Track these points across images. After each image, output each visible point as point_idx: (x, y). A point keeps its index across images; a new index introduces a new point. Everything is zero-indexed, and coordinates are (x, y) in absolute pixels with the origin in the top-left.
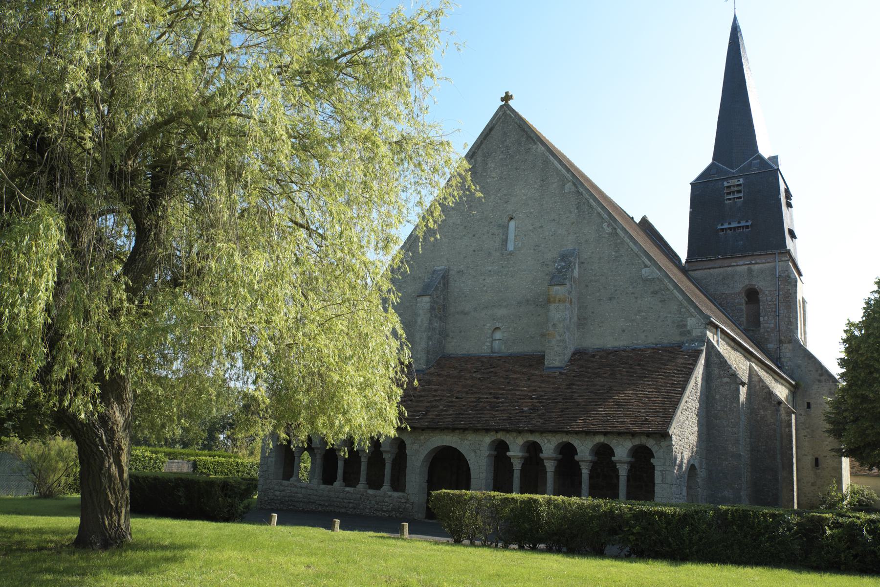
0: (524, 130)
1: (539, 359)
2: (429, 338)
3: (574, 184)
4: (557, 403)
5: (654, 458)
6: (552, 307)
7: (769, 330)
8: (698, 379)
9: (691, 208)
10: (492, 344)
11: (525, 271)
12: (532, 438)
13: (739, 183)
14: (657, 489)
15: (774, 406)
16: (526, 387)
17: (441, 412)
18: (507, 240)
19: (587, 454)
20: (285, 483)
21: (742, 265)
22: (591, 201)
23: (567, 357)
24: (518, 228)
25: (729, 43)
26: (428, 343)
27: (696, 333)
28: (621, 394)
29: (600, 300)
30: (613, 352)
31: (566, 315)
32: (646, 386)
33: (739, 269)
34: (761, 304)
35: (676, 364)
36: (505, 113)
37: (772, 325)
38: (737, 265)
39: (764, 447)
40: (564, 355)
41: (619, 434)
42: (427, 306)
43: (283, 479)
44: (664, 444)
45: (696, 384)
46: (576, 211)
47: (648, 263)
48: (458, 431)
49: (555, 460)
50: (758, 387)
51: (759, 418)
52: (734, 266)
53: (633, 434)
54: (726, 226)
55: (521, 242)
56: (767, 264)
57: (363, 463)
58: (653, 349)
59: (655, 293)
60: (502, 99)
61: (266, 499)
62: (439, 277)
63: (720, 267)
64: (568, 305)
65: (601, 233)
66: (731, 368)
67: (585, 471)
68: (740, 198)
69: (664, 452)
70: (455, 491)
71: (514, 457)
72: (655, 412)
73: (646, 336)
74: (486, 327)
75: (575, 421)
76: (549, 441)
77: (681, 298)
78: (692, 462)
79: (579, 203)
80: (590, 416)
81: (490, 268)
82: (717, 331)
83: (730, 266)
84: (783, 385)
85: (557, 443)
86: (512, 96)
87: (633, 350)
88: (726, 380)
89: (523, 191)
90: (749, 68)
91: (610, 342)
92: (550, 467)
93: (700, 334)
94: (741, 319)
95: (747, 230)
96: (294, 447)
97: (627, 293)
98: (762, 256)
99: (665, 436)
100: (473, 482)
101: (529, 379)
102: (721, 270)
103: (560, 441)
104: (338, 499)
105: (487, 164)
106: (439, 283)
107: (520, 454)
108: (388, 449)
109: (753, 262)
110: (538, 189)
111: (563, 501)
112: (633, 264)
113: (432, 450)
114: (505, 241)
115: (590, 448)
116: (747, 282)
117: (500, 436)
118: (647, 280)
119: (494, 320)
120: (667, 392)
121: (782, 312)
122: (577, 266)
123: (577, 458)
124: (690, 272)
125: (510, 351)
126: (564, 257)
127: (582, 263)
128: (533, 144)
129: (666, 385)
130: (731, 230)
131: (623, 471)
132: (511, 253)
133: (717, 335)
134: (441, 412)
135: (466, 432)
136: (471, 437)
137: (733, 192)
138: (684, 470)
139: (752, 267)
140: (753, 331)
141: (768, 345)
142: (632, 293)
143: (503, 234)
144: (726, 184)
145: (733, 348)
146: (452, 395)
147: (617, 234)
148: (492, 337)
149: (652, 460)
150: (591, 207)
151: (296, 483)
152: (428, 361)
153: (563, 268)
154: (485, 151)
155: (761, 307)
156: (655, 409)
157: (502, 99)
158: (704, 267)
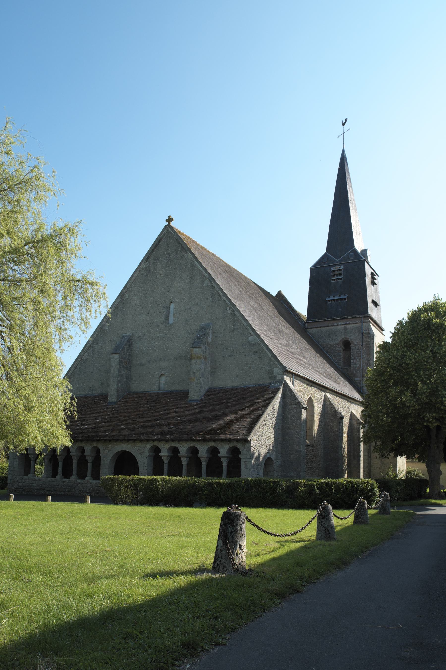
0: (179, 243)
1: (184, 395)
2: (119, 382)
3: (210, 281)
4: (191, 423)
5: (241, 454)
6: (193, 361)
7: (356, 368)
8: (275, 406)
9: (310, 285)
10: (159, 385)
11: (179, 337)
12: (173, 444)
13: (340, 269)
14: (242, 472)
15: (338, 420)
16: (175, 413)
17: (122, 430)
18: (169, 317)
19: (205, 453)
20: (26, 477)
21: (340, 325)
22: (220, 292)
23: (202, 394)
24: (175, 309)
25: (339, 169)
26: (118, 385)
27: (278, 377)
28: (228, 417)
29: (224, 357)
30: (231, 390)
31: (201, 367)
32: (243, 412)
33: (339, 327)
34: (352, 351)
35: (264, 398)
36: (168, 231)
37: (358, 365)
38: (338, 325)
39: (332, 446)
40: (200, 392)
41: (222, 441)
42: (117, 361)
43: (24, 475)
44: (246, 446)
45: (273, 409)
46: (211, 299)
47: (252, 333)
48: (131, 441)
49: (187, 457)
50: (329, 408)
51: (329, 428)
52: (336, 325)
53: (230, 441)
54: (331, 298)
55: (177, 318)
56: (356, 325)
57: (74, 463)
58: (253, 387)
59: (256, 352)
60: (167, 221)
61: (13, 488)
62: (126, 341)
63: (327, 326)
64: (203, 360)
65: (225, 314)
66: (297, 399)
67: (204, 464)
68: (341, 279)
69: (246, 450)
70: (115, 476)
71: (164, 456)
72: (244, 427)
73: (250, 380)
74: (156, 374)
75: (198, 434)
76: (183, 446)
77: (270, 355)
78: (268, 456)
79: (212, 293)
80: (208, 430)
81: (158, 335)
82: (293, 376)
83: (334, 325)
84: (355, 404)
85: (188, 447)
86: (172, 219)
87: (242, 388)
88: (294, 406)
89: (179, 284)
90: (351, 187)
91: (230, 383)
92: (184, 461)
93: (280, 378)
94: (339, 361)
95: (345, 301)
96: (19, 453)
97: (240, 352)
98: (353, 319)
99: (246, 442)
100: (139, 473)
101: (178, 408)
102: (328, 328)
103: (190, 446)
104: (59, 487)
105: (156, 265)
106: (125, 345)
107: (167, 454)
108: (89, 454)
109: (348, 323)
110: (188, 283)
111: (169, 479)
112: (244, 334)
113: (115, 453)
114: (168, 317)
115: (206, 449)
116: (343, 336)
117: (155, 443)
118: (252, 344)
119: (160, 369)
120: (254, 415)
121: (364, 356)
122: (210, 334)
123: (199, 455)
124: (308, 330)
125: (170, 389)
126: (203, 329)
127: (214, 332)
128: (185, 252)
129: (254, 410)
130: (334, 301)
131: (225, 462)
132: (171, 325)
133: (292, 378)
134: (122, 430)
135: (136, 442)
136: (139, 445)
137: (337, 275)
138: (261, 460)
139: (347, 326)
140: (346, 369)
141: (356, 379)
142: (243, 352)
143: (166, 313)
144: (332, 269)
145: (308, 385)
146: (131, 419)
147: (235, 314)
148: (159, 381)
149: (240, 456)
150: (219, 296)
151: (32, 478)
152: (118, 396)
153: (201, 336)
154: (155, 256)
155: (352, 353)
156: (244, 425)
157: (167, 221)
158: (317, 326)
